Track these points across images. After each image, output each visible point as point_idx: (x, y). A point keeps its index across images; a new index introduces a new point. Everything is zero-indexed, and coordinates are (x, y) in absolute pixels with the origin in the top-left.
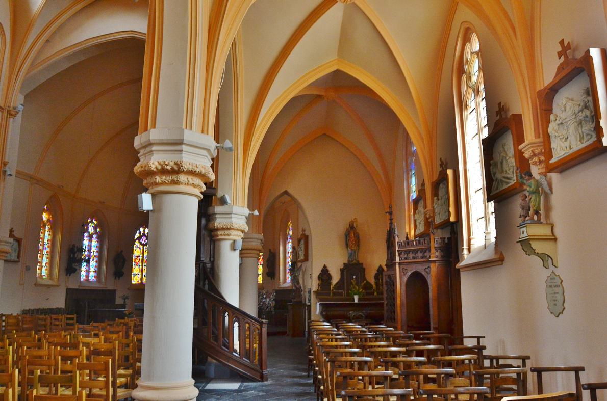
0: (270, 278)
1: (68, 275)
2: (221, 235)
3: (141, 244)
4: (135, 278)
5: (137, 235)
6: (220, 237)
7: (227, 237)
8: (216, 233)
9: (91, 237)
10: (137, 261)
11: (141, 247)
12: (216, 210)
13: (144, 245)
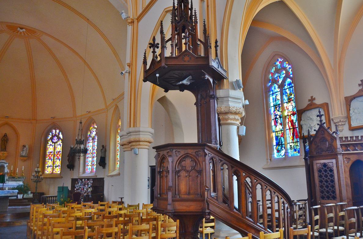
0: (69, 169)
1: (72, 170)
2: (231, 119)
3: (53, 142)
4: (56, 169)
5: (50, 136)
6: (229, 121)
7: (235, 122)
8: (226, 117)
9: (93, 139)
10: (50, 156)
11: (53, 144)
12: (230, 94)
13: (55, 143)
